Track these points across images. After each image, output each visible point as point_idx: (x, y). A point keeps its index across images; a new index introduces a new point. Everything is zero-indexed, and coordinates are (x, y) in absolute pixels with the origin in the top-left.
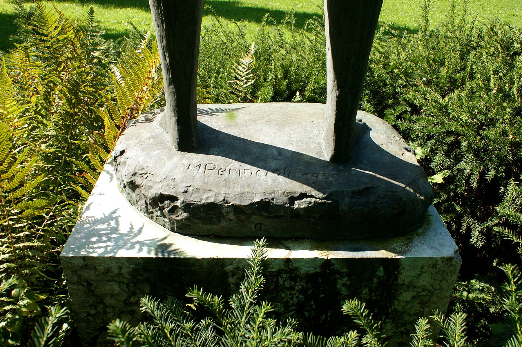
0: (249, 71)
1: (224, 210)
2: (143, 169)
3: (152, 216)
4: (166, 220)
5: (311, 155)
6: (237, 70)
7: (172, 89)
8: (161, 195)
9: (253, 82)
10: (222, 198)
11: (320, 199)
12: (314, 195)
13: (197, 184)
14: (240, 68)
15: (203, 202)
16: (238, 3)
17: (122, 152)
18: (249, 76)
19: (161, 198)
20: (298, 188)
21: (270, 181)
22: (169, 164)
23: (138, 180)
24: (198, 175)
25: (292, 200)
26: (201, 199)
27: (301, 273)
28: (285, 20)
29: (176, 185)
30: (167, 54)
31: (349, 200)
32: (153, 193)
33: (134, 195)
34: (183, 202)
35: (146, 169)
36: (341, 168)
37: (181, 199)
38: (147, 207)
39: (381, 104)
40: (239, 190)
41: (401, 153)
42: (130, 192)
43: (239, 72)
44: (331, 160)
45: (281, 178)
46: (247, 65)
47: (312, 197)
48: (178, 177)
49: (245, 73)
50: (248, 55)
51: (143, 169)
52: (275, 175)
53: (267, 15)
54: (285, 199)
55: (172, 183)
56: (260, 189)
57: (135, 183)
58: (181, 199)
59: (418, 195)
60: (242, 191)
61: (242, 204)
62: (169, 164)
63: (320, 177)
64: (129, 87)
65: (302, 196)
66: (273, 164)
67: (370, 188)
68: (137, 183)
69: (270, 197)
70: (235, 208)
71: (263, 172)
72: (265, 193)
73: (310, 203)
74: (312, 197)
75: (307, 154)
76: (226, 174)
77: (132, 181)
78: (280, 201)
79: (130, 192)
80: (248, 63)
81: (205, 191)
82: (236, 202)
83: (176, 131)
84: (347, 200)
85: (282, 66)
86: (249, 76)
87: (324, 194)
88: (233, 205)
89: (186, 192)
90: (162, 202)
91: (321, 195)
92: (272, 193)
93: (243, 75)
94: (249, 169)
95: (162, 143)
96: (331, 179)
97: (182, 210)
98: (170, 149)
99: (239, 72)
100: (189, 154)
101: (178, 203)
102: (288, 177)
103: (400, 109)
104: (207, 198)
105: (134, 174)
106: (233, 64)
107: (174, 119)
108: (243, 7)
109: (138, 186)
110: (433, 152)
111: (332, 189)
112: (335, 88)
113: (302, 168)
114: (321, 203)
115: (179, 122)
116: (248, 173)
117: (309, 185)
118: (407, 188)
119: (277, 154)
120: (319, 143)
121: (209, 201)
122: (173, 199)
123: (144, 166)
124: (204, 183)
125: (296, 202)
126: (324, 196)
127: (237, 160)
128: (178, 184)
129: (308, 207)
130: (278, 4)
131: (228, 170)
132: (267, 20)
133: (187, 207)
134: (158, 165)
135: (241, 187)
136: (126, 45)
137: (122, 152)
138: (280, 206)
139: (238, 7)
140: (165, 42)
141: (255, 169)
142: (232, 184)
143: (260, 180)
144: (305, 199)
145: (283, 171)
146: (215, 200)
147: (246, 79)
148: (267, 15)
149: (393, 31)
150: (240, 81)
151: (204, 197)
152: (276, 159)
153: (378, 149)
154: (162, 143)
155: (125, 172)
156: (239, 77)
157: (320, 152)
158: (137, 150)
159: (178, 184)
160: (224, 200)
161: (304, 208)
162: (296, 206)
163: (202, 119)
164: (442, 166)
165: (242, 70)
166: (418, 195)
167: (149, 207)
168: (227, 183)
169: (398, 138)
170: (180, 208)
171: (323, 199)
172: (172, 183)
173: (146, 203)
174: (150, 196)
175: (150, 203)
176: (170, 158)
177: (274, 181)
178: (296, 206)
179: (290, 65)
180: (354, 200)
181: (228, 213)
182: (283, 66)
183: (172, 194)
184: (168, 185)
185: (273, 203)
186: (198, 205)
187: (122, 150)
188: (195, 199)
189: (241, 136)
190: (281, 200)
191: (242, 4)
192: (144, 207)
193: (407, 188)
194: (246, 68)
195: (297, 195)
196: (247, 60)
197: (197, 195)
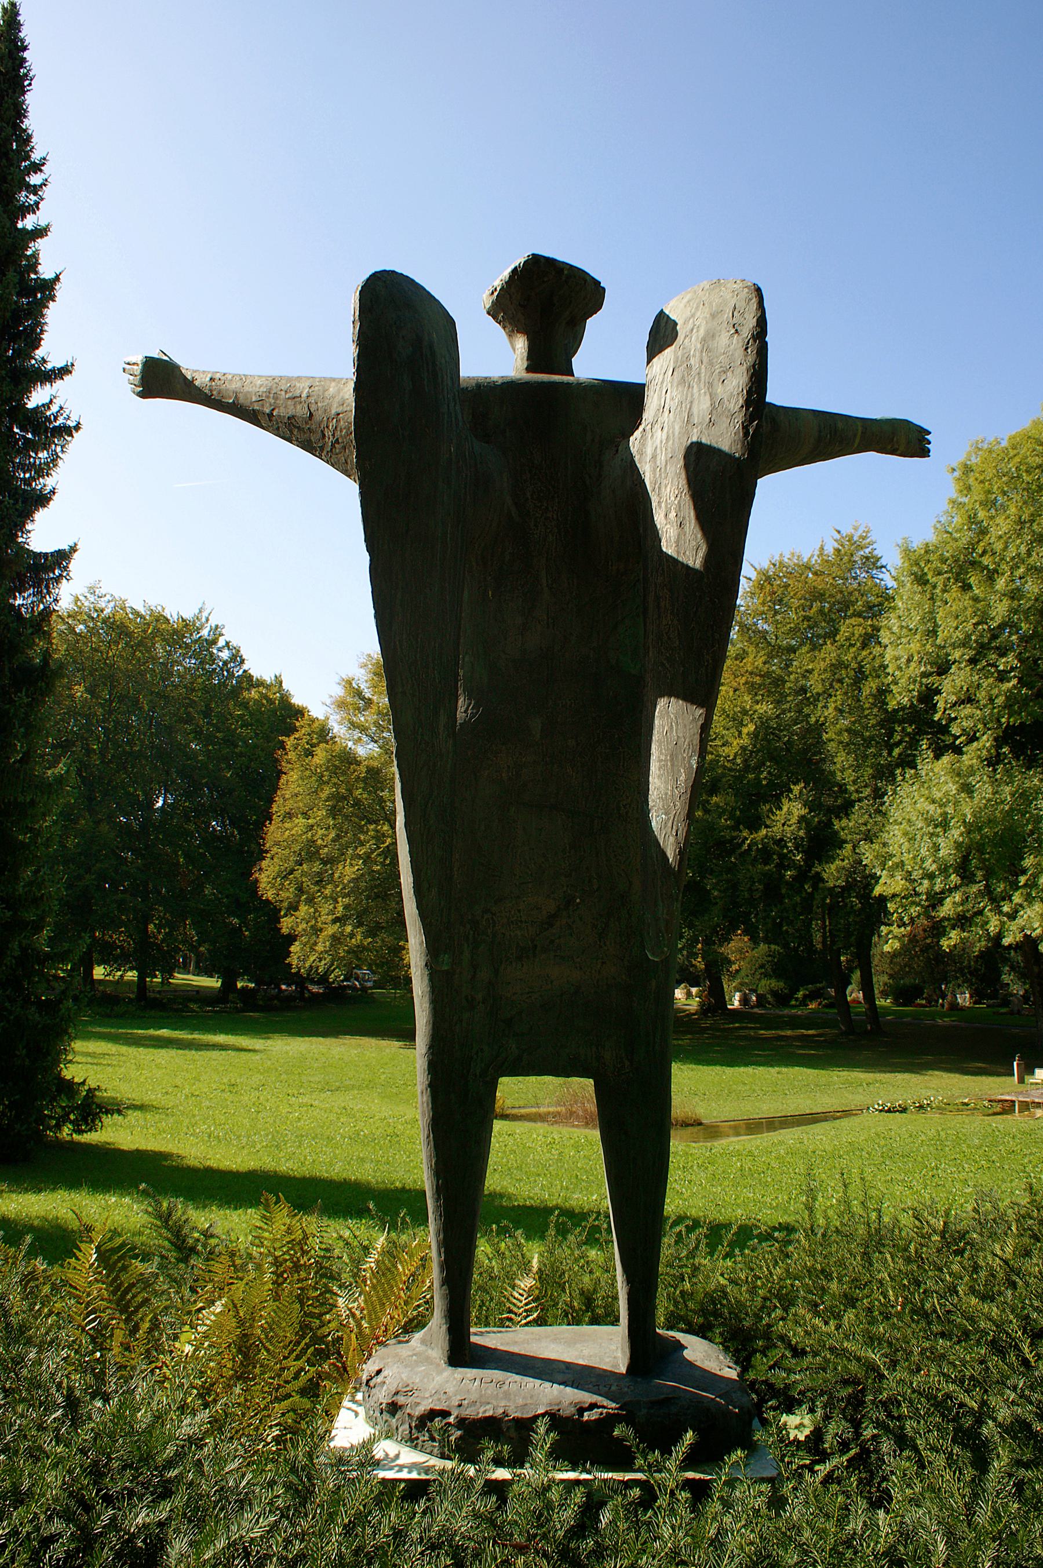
0: (530, 1299)
1: (503, 1425)
2: (408, 1386)
3: (417, 1444)
4: (435, 1444)
5: (604, 1368)
6: (511, 1298)
7: (445, 1290)
8: (432, 1411)
9: (535, 1315)
10: (501, 1411)
11: (612, 1409)
12: (605, 1404)
13: (474, 1397)
14: (517, 1295)
15: (480, 1415)
16: (501, 1196)
17: (379, 1372)
18: (530, 1306)
19: (432, 1414)
20: (587, 1398)
21: (555, 1393)
22: (439, 1379)
23: (401, 1400)
24: (474, 1388)
25: (581, 1411)
26: (478, 1413)
27: (595, 1500)
28: (588, 1222)
29: (449, 1399)
30: (443, 1250)
31: (646, 1411)
32: (418, 1411)
33: (394, 1420)
34: (457, 1417)
35: (411, 1385)
36: (639, 1380)
37: (455, 1413)
38: (410, 1432)
39: (746, 1350)
40: (521, 1402)
41: (718, 1369)
42: (388, 1418)
43: (515, 1301)
44: (627, 1372)
45: (568, 1389)
46: (526, 1289)
47: (604, 1407)
48: (450, 1390)
49: (524, 1302)
50: (527, 1275)
51: (408, 1386)
52: (562, 1387)
53: (556, 1212)
54: (573, 1410)
55: (444, 1397)
56: (545, 1401)
57: (397, 1403)
58: (455, 1413)
59: (730, 1407)
60: (525, 1402)
61: (524, 1416)
62: (439, 1379)
63: (613, 1388)
64: (380, 1300)
65: (593, 1406)
66: (560, 1377)
67: (671, 1398)
68: (400, 1403)
69: (557, 1408)
70: (516, 1420)
71: (548, 1384)
72: (551, 1404)
73: (601, 1414)
74: (604, 1407)
75: (601, 1367)
76: (506, 1387)
77: (393, 1402)
78: (568, 1412)
79: (388, 1418)
80: (529, 1286)
81: (482, 1404)
82: (518, 1415)
83: (447, 1342)
84: (644, 1411)
85: (582, 1293)
86: (530, 1306)
87: (617, 1403)
88: (514, 1418)
89: (460, 1405)
90: (432, 1421)
91: (614, 1405)
92: (558, 1405)
93: (519, 1304)
94: (532, 1383)
95: (428, 1360)
96: (626, 1389)
97: (456, 1427)
98: (438, 1365)
99: (515, 1301)
100: (460, 1369)
101: (451, 1419)
102: (577, 1388)
103: (775, 1354)
104: (485, 1412)
105: (397, 1393)
106: (506, 1289)
107: (444, 1327)
108: (514, 1206)
109: (401, 1407)
110: (827, 1418)
111: (627, 1399)
112: (625, 1284)
113: (593, 1380)
114: (614, 1413)
115: (450, 1330)
116: (532, 1385)
117: (600, 1395)
118: (718, 1399)
119: (564, 1367)
120: (615, 1357)
121: (487, 1415)
122: (445, 1414)
123: (410, 1382)
124: (481, 1396)
125: (585, 1414)
126: (617, 1406)
127: (517, 1374)
128: (451, 1397)
129: (599, 1419)
130: (594, 1198)
131: (507, 1383)
132: (557, 1221)
133: (461, 1423)
134: (426, 1380)
135: (523, 1398)
136: (155, 1326)
137: (379, 1372)
138: (567, 1418)
139: (502, 1206)
140: (441, 1236)
141: (539, 1381)
142: (512, 1396)
143: (544, 1392)
144: (596, 1410)
145: (570, 1383)
146: (494, 1413)
147: (526, 1311)
148: (556, 1212)
149: (776, 1234)
150: (516, 1314)
151: (481, 1410)
152: (564, 1372)
153: (691, 1365)
154: (428, 1360)
155: (382, 1395)
156: (515, 1309)
157: (617, 1366)
158: (398, 1367)
159: (451, 1397)
160: (504, 1413)
161: (595, 1420)
162: (586, 1418)
163: (473, 1339)
164: (839, 1437)
165: (520, 1297)
166: (730, 1407)
167: (414, 1431)
168: (507, 1395)
169: (721, 1357)
170: (453, 1425)
171: (616, 1409)
172: (444, 1397)
173: (410, 1427)
174: (417, 1414)
175: (416, 1425)
176: (440, 1373)
177: (560, 1392)
178: (586, 1418)
179: (594, 1289)
180: (652, 1411)
181: (508, 1428)
182: (583, 1292)
183: (445, 1408)
184: (439, 1399)
185: (559, 1415)
186: (474, 1419)
187: (377, 1368)
188: (470, 1413)
189: (523, 1352)
190: (568, 1411)
191: (509, 1198)
192: (408, 1432)
193: (718, 1399)
194: (524, 1293)
195: (587, 1405)
196: (527, 1283)
197: (473, 1408)
